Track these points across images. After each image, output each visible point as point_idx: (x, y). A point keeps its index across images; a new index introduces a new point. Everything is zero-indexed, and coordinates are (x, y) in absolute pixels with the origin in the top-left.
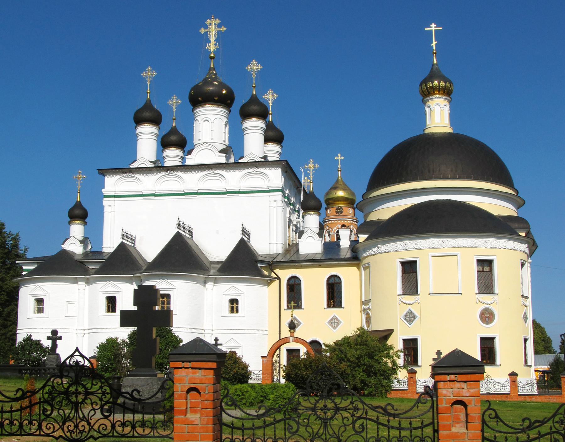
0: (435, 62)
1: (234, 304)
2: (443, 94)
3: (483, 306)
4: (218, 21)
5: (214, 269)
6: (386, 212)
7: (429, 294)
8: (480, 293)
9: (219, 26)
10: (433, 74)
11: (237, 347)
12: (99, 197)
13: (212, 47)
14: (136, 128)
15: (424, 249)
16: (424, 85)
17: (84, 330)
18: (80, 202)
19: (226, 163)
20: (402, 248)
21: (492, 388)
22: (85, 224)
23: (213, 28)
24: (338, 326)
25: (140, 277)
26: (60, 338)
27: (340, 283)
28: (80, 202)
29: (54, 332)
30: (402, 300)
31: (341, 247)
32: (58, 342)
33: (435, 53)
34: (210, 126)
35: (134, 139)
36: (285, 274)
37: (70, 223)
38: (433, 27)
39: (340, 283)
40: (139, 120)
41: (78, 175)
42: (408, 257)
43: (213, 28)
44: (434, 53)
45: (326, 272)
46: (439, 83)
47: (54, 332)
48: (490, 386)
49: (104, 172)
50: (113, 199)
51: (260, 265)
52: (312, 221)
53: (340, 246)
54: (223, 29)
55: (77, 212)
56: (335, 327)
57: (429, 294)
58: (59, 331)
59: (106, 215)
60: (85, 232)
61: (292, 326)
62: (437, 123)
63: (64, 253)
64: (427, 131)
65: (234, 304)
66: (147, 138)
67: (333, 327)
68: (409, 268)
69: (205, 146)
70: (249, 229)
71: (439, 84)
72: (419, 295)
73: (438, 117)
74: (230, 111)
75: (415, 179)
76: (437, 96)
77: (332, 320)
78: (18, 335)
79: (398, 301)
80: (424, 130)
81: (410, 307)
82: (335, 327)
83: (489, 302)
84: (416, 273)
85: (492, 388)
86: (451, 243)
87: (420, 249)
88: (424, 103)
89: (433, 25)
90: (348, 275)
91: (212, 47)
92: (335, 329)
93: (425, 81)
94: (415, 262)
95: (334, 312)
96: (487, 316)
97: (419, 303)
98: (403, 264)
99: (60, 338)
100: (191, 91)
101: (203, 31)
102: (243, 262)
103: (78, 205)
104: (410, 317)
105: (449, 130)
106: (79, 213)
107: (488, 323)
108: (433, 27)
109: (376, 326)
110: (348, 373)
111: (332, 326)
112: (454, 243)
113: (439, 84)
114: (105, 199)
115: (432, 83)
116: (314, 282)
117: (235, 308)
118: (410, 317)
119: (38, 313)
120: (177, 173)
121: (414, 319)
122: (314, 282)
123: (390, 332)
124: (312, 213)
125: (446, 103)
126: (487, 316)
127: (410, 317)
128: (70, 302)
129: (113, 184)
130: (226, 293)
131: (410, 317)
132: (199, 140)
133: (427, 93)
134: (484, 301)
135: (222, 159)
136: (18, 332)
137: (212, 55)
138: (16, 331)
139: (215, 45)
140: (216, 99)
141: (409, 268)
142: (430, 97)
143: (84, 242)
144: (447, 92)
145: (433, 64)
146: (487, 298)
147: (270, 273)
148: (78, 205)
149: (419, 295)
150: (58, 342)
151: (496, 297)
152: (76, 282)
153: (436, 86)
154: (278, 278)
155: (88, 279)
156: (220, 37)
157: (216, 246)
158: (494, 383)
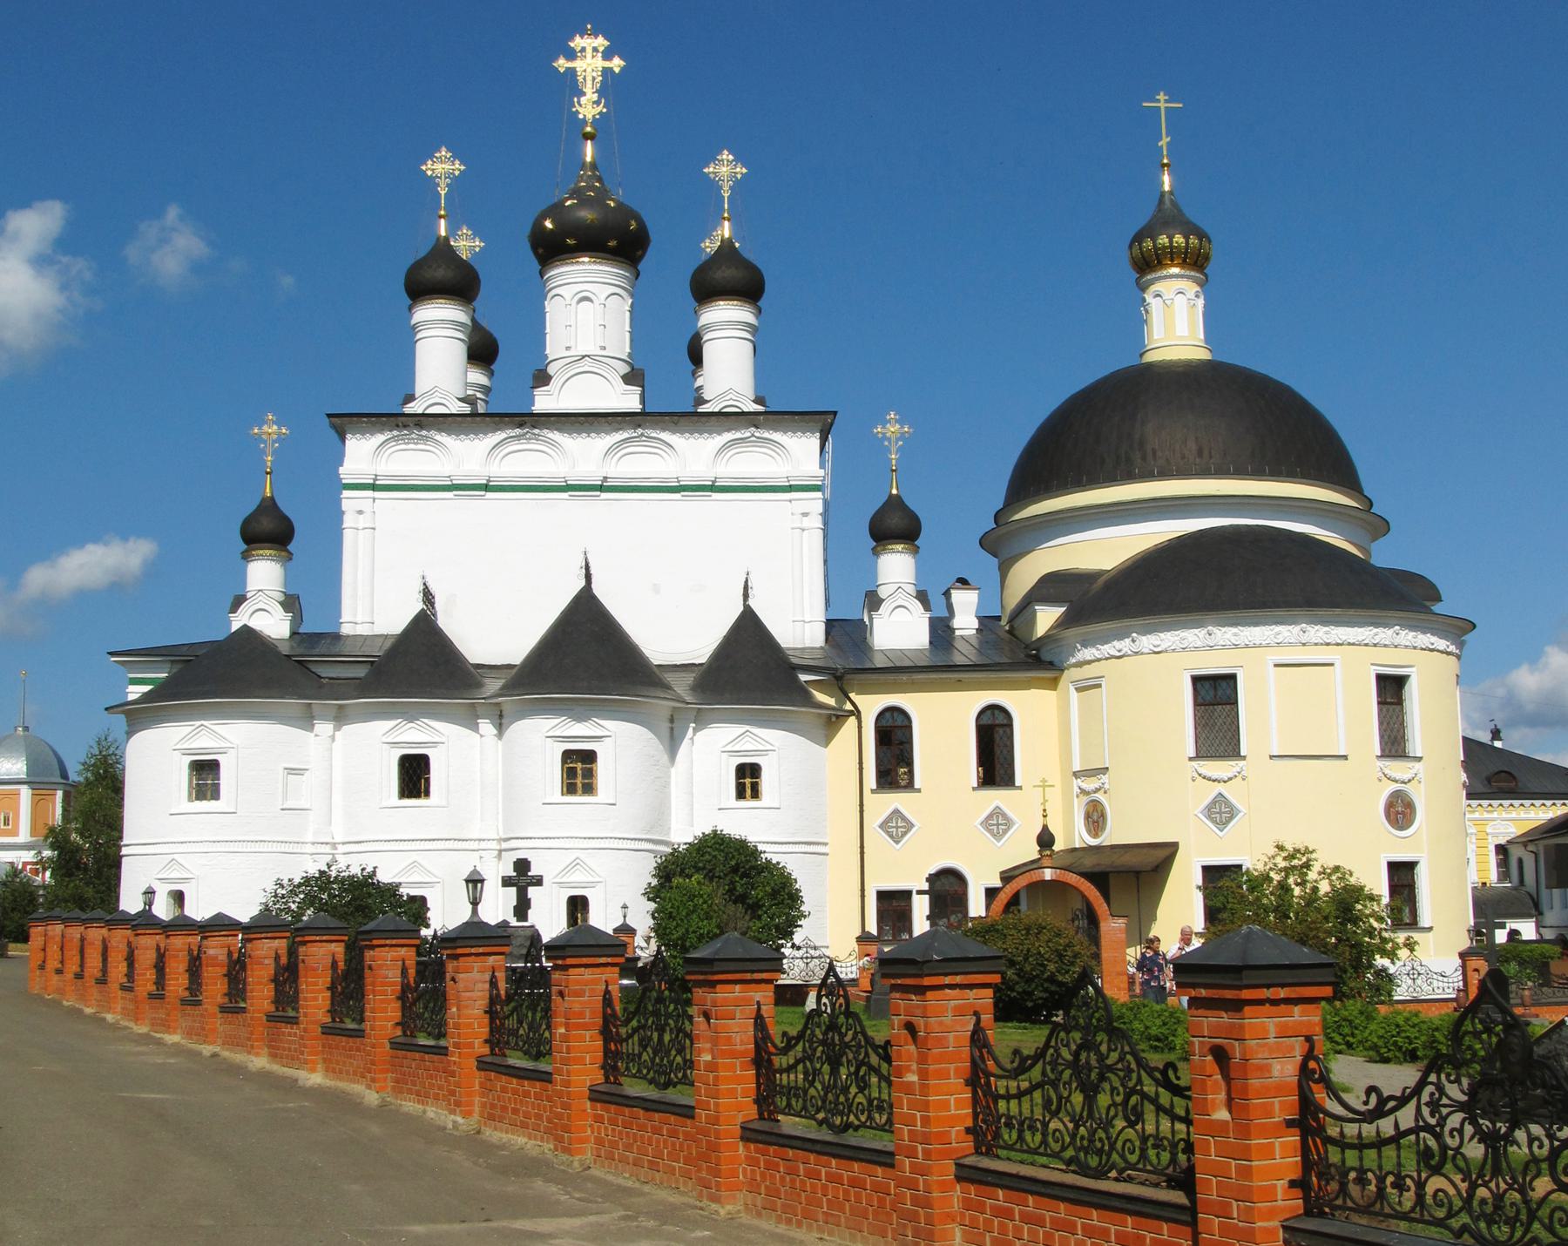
0: (1167, 188)
1: (414, 776)
2: (1184, 264)
3: (1395, 787)
4: (601, 42)
5: (681, 685)
6: (1104, 550)
7: (1272, 757)
8: (1382, 756)
9: (607, 55)
10: (1167, 216)
11: (591, 885)
12: (329, 489)
13: (588, 107)
14: (410, 308)
15: (1255, 650)
16: (1148, 244)
17: (334, 845)
18: (272, 498)
19: (643, 414)
20: (1199, 644)
21: (1425, 987)
22: (915, 551)
23: (590, 59)
24: (1005, 832)
25: (498, 704)
26: (538, 881)
27: (1009, 725)
28: (272, 498)
29: (522, 866)
30: (1201, 771)
31: (957, 633)
32: (532, 892)
33: (1167, 165)
34: (586, 313)
35: (407, 339)
36: (871, 705)
37: (246, 556)
38: (1162, 101)
39: (1010, 725)
40: (420, 289)
41: (265, 428)
42: (1213, 665)
43: (590, 59)
44: (1164, 165)
45: (969, 703)
46: (1171, 238)
47: (522, 866)
48: (1419, 982)
49: (344, 423)
50: (369, 493)
51: (803, 677)
52: (896, 567)
53: (953, 630)
54: (617, 64)
55: (895, 521)
56: (998, 836)
57: (1345, 757)
58: (1473, 877)
59: (348, 536)
60: (288, 580)
61: (1046, 838)
62: (1181, 338)
63: (248, 634)
64: (1151, 357)
65: (414, 776)
66: (439, 333)
67: (994, 835)
68: (1215, 695)
69: (586, 365)
70: (433, 588)
71: (1171, 241)
72: (1244, 758)
73: (1176, 322)
74: (637, 275)
75: (1130, 477)
76: (1175, 270)
77: (990, 817)
78: (124, 860)
79: (1190, 774)
80: (1141, 355)
81: (1220, 788)
82: (998, 836)
83: (1406, 777)
84: (1236, 703)
85: (1425, 987)
86: (1320, 634)
87: (1247, 646)
88: (1143, 288)
89: (1162, 97)
90: (1029, 707)
91: (588, 107)
92: (897, 842)
93: (1138, 238)
94: (1232, 678)
95: (996, 797)
96: (1400, 811)
97: (1249, 779)
98: (1381, 679)
99: (538, 881)
100: (543, 216)
101: (562, 64)
102: (749, 671)
103: (269, 507)
104: (1221, 812)
105: (1203, 355)
106: (269, 531)
107: (1402, 828)
108: (1162, 101)
109: (1117, 833)
110: (1033, 954)
111: (990, 831)
112: (1235, 635)
113: (1171, 241)
114: (346, 493)
115: (1171, 238)
116: (943, 723)
117: (748, 786)
118: (1221, 812)
119: (198, 798)
120: (550, 435)
121: (1231, 818)
122: (943, 723)
123: (1172, 848)
124: (900, 547)
125: (1191, 288)
126: (1400, 811)
127: (1220, 813)
128: (292, 771)
129: (363, 455)
130: (729, 748)
131: (1220, 813)
132: (568, 348)
133: (1147, 264)
134: (1209, 774)
135: (630, 400)
136: (124, 851)
137: (589, 129)
138: (120, 848)
139: (597, 103)
140: (612, 243)
141: (1215, 695)
142: (1159, 274)
143: (291, 603)
144: (1195, 261)
145: (1163, 194)
146: (1397, 769)
147: (840, 702)
148: (269, 507)
149: (1244, 758)
150: (532, 892)
151: (1241, 763)
152: (306, 721)
153: (1164, 247)
154: (857, 713)
155: (341, 706)
156: (610, 85)
157: (674, 628)
158: (1429, 975)
